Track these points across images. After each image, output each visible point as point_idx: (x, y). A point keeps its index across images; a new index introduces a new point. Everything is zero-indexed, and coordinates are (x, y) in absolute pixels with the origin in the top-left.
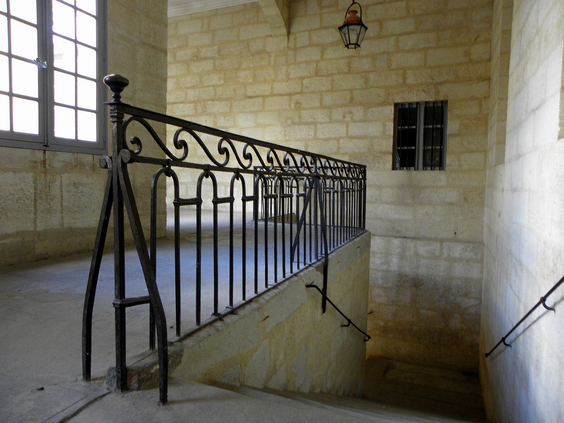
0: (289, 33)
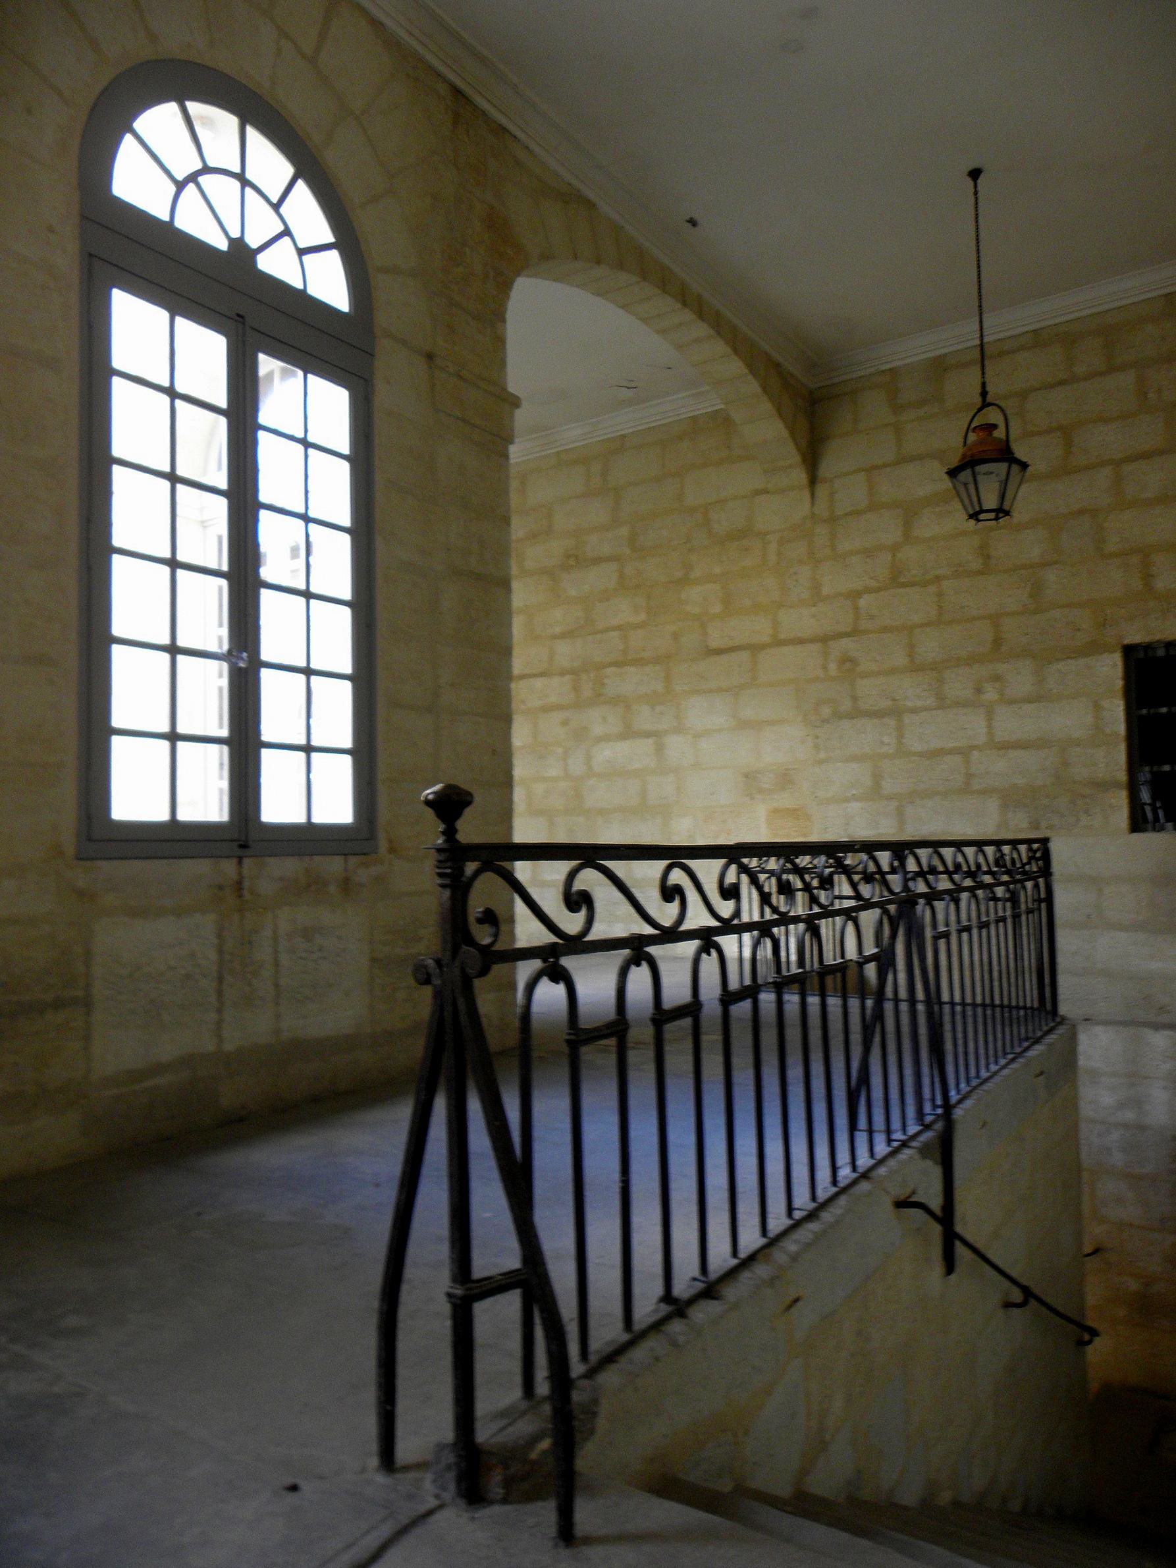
0: (813, 481)
